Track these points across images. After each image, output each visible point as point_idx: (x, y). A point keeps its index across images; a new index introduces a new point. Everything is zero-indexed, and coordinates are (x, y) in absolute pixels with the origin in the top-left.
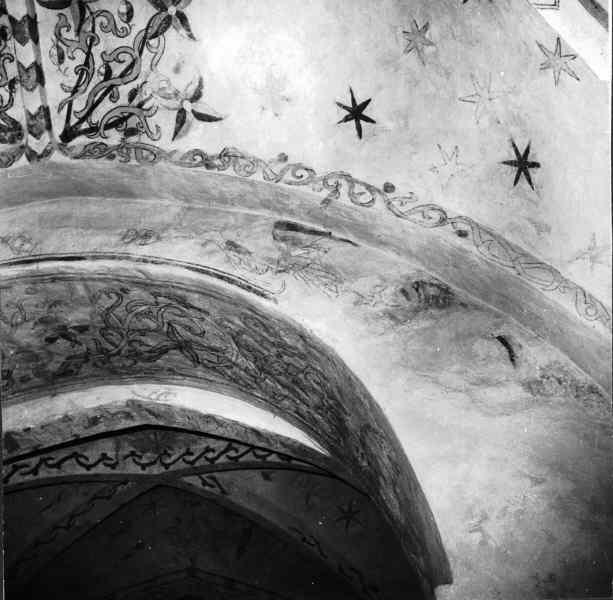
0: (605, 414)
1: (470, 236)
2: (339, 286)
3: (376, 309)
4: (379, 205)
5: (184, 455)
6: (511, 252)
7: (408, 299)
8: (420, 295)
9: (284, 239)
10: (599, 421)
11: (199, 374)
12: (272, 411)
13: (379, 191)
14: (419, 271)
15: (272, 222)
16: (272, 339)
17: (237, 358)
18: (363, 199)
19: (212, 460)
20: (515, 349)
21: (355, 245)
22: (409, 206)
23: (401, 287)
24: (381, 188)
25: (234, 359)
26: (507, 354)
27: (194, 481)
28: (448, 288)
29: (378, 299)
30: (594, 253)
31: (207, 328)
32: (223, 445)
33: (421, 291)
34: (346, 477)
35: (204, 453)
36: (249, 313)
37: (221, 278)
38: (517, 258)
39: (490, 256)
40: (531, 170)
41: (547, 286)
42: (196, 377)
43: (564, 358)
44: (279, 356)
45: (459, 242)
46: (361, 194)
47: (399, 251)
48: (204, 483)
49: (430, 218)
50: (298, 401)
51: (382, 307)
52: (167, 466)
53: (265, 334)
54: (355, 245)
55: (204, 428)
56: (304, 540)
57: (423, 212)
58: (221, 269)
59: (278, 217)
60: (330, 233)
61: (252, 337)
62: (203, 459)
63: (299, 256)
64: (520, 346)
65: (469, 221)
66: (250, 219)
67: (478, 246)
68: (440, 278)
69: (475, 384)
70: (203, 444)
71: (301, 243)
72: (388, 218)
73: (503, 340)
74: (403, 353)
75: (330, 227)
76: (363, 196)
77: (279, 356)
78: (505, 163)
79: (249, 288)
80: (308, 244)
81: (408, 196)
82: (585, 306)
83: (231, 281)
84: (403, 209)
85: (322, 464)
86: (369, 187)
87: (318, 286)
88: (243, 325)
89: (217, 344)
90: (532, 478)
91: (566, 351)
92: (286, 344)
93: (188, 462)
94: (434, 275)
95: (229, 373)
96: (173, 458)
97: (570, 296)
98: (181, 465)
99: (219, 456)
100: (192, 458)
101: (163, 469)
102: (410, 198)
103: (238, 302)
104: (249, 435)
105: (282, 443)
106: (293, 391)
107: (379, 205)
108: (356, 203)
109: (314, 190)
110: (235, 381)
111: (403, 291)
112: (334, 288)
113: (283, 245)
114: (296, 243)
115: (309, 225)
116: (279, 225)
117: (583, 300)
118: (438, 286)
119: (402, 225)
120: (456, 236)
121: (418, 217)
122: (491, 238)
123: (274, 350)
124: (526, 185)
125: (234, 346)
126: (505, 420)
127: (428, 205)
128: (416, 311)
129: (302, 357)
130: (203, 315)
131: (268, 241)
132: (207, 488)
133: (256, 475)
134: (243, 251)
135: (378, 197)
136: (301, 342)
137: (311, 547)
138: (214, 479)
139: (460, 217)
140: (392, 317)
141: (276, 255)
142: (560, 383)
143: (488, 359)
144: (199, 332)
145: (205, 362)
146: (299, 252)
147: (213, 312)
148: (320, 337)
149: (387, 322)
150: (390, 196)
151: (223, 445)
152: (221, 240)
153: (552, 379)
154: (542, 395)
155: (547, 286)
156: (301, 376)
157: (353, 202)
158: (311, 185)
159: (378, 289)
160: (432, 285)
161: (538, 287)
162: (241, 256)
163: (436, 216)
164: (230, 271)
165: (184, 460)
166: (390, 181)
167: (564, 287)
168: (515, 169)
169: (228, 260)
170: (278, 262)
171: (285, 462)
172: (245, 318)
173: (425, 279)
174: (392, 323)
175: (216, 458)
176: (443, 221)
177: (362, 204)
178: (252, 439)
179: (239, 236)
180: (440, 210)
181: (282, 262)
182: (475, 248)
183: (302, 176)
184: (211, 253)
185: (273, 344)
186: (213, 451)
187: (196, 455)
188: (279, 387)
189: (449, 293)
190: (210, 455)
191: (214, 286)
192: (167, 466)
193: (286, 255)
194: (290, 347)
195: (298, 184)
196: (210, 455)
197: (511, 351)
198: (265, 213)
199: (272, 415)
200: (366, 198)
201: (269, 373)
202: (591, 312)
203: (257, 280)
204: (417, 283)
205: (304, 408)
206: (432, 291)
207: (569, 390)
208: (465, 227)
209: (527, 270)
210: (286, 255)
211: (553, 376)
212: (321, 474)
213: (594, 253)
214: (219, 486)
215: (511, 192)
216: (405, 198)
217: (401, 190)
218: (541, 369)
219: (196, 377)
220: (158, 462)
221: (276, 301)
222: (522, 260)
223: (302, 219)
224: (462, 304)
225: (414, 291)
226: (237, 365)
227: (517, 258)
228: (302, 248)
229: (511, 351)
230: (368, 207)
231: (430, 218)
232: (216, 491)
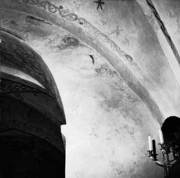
0: (117, 79)
1: (83, 24)
2: (44, 37)
3: (55, 45)
4: (57, 13)
5: (9, 87)
6: (95, 30)
7: (65, 42)
8: (69, 42)
9: (29, 22)
10: (115, 82)
11: (7, 62)
12: (29, 75)
13: (58, 8)
14: (69, 34)
15: (26, 16)
16: (25, 52)
17: (17, 58)
18: (53, 10)
19: (17, 89)
20: (95, 59)
21: (51, 25)
22: (67, 14)
23: (63, 38)
24: (59, 7)
25: (16, 58)
26: (92, 60)
27: (13, 95)
28: (77, 40)
29: (56, 42)
30: (118, 31)
31: (6, 48)
32: (20, 85)
33: (69, 40)
34: (50, 95)
35: (15, 87)
36: (17, 43)
37: (8, 32)
38: (96, 32)
39: (88, 31)
40: (102, 5)
41: (104, 41)
42: (6, 63)
43: (108, 63)
44: (27, 57)
45: (80, 26)
46: (52, 9)
47: (64, 28)
48: (16, 96)
49: (72, 18)
50: (35, 72)
51: (56, 44)
52: (4, 90)
53: (23, 51)
54: (51, 25)
55: (9, 79)
56: (46, 113)
57: (70, 16)
58: (8, 29)
59: (28, 15)
60: (44, 21)
61: (20, 51)
62: (8, 89)
63: (33, 27)
64: (96, 58)
65: (84, 20)
66: (19, 15)
67: (85, 27)
68: (76, 37)
69: (81, 69)
70: (15, 84)
71: (34, 23)
72: (59, 17)
73: (91, 56)
74: (163, 72)
75: (44, 19)
76: (53, 10)
77: (27, 57)
78: (95, 2)
79: (16, 36)
80: (37, 23)
81: (67, 10)
82: (114, 47)
83: (11, 34)
84: (64, 14)
85: (44, 91)
86: (55, 7)
87: (38, 37)
88: (16, 47)
89: (10, 53)
90: (93, 97)
91: (109, 60)
92: (28, 54)
93: (16, 89)
94: (74, 36)
95: (15, 62)
96: (6, 88)
97: (110, 44)
98: (8, 90)
99: (19, 88)
100: (11, 88)
101: (3, 91)
102: (67, 11)
103: (13, 40)
104: (23, 81)
105: (32, 84)
106: (33, 69)
107: (57, 13)
108: (50, 11)
109: (38, 6)
110: (18, 65)
111: (64, 40)
112: (43, 38)
113: (29, 23)
114: (33, 23)
115: (38, 18)
116: (28, 17)
117: (113, 45)
118: (74, 39)
119: (64, 20)
120: (79, 23)
121: (68, 17)
122: (89, 25)
123: (26, 56)
124: (101, 10)
125: (15, 54)
126: (88, 79)
127: (72, 14)
128: (67, 46)
129: (34, 58)
130: (5, 44)
131: (24, 22)
132: (17, 97)
133: (32, 94)
134: (16, 24)
135: (57, 10)
136: (32, 53)
137: (47, 116)
138: (19, 95)
139: (81, 18)
140: (59, 47)
141: (26, 26)
142: (106, 70)
143: (85, 62)
144: (4, 49)
145: (8, 59)
146: (33, 26)
147: (8, 43)
148: (37, 52)
149: (58, 49)
150: (61, 10)
151: (20, 85)
152: (9, 20)
153: (104, 69)
154: (100, 73)
155: (104, 41)
156: (34, 64)
157: (49, 11)
158: (37, 5)
159: (56, 39)
160: (73, 38)
161: (101, 41)
162: (15, 26)
163: (74, 17)
164: (11, 30)
165: (15, 88)
166: (62, 5)
167: (108, 41)
168: (98, 4)
169: (11, 27)
170: (27, 28)
171: (31, 90)
172: (17, 46)
173: (71, 36)
174: (59, 49)
175: (19, 89)
176: (76, 19)
177: (52, 12)
178: (23, 83)
179: (15, 19)
180: (76, 15)
181: (28, 29)
182: (84, 28)
183: (35, 2)
184: (7, 24)
185: (25, 53)
186: (18, 86)
187: (13, 87)
188: (29, 67)
189: (78, 41)
190: (17, 88)
191: (6, 34)
192: (4, 90)
193: (29, 26)
194: (30, 55)
195: (33, 4)
196: (17, 88)
197: (93, 60)
198: (25, 13)
199: (29, 76)
200: (53, 10)
201: (25, 63)
202: (115, 49)
203: (18, 33)
204: (68, 38)
205: (36, 74)
206: (72, 40)
207: (108, 72)
208: (81, 21)
209: (98, 36)
210: (29, 26)
211: (104, 68)
212: (42, 93)
213: (118, 31)
214: (21, 97)
215: (96, 11)
216: (65, 11)
217: (65, 8)
218: (101, 65)
219: (6, 63)
220: (2, 89)
221: (24, 41)
222: (98, 32)
223: (35, 15)
224: (81, 45)
225: (67, 40)
226: (17, 60)
227: (96, 32)
228: (35, 25)
229: (93, 60)
230: (54, 13)
231: (72, 18)
232: (20, 98)
